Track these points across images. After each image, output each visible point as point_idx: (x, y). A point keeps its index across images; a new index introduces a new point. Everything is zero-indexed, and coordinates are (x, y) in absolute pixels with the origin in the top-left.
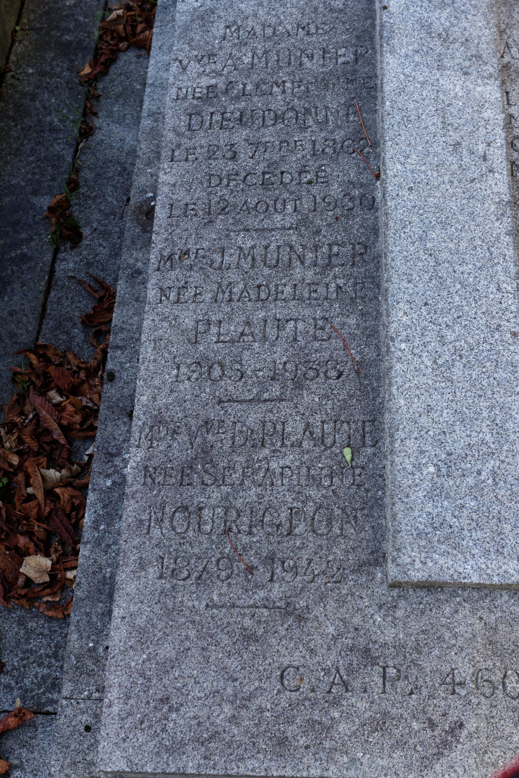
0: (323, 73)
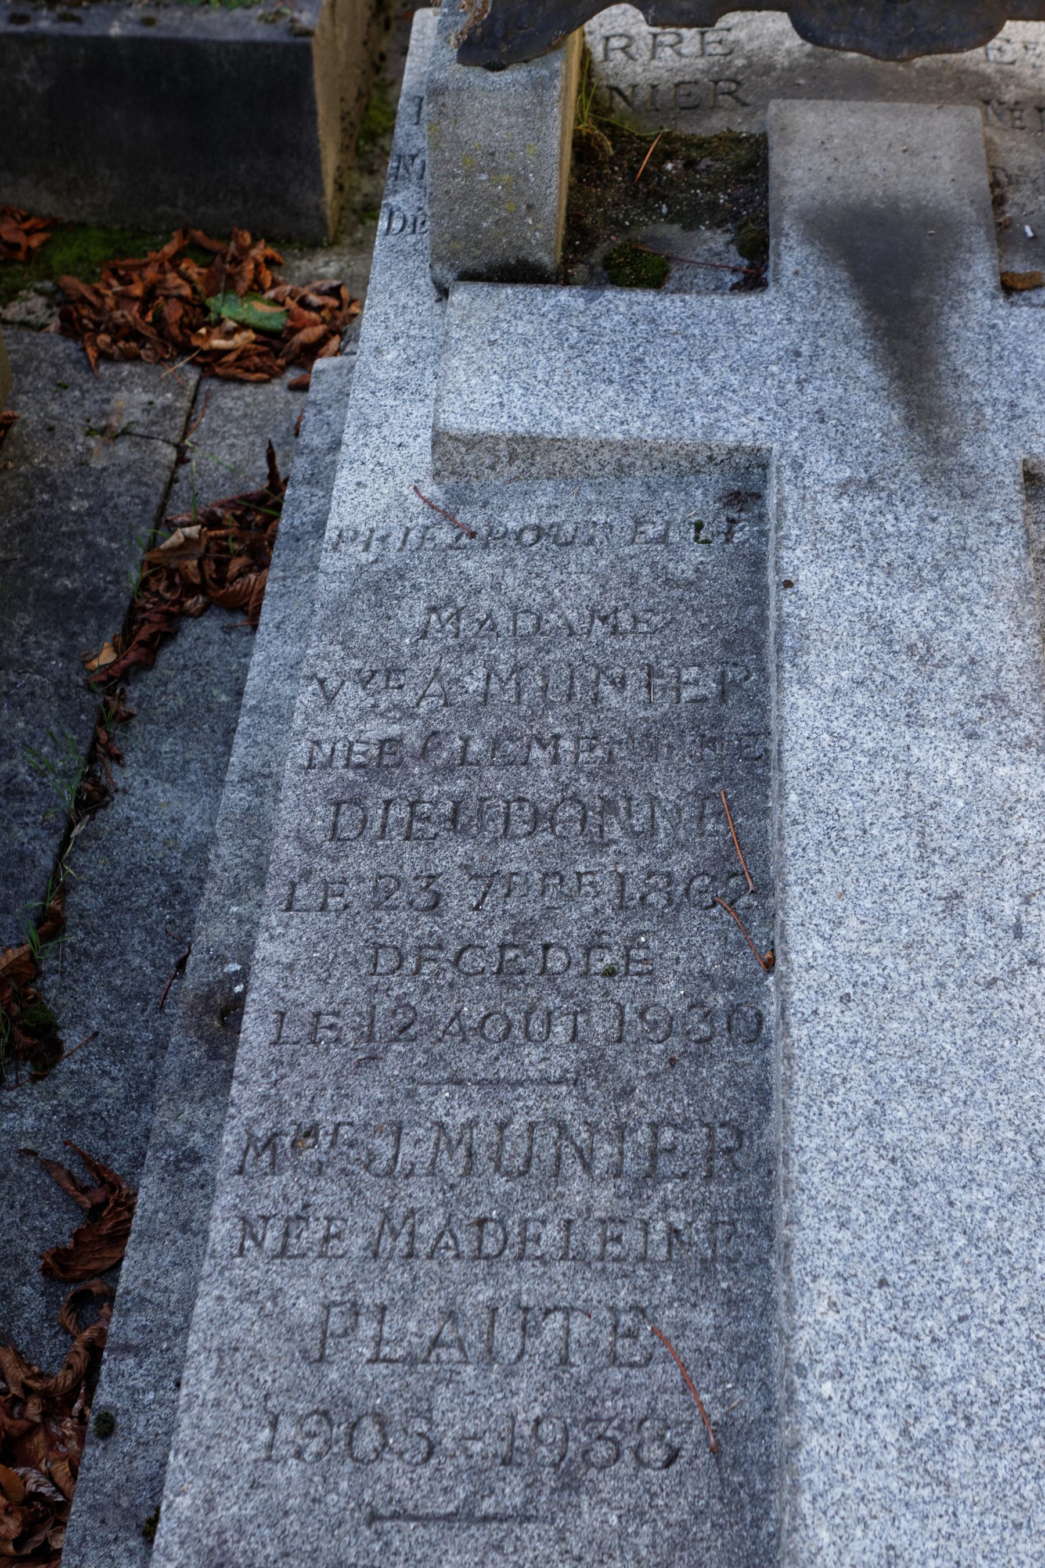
0: (646, 719)
